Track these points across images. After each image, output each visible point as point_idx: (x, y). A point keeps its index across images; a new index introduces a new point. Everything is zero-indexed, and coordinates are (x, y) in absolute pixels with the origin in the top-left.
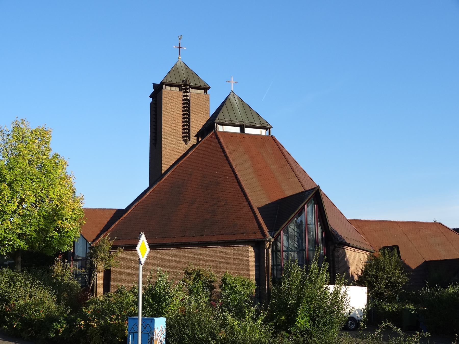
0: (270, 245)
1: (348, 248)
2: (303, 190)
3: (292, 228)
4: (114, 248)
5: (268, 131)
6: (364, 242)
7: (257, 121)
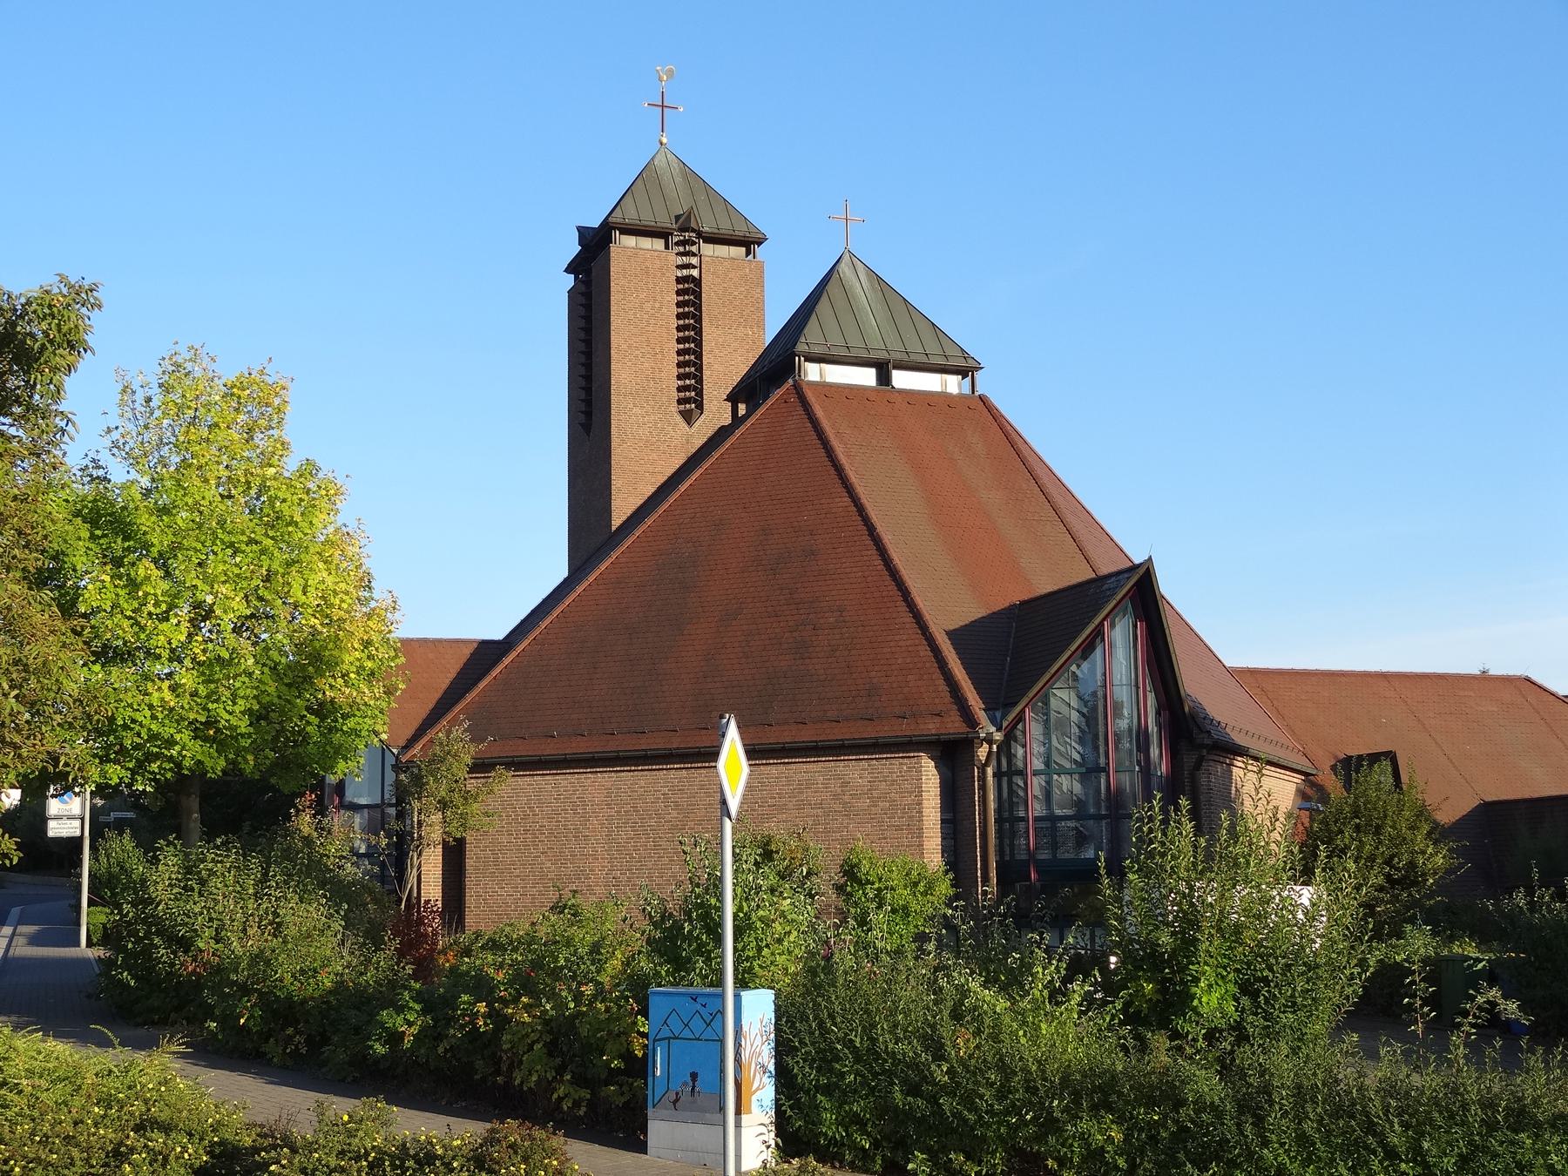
0: (990, 753)
1: (1239, 762)
2: (1084, 574)
3: (1063, 699)
4: (481, 767)
5: (968, 379)
6: (1286, 742)
7: (933, 347)
